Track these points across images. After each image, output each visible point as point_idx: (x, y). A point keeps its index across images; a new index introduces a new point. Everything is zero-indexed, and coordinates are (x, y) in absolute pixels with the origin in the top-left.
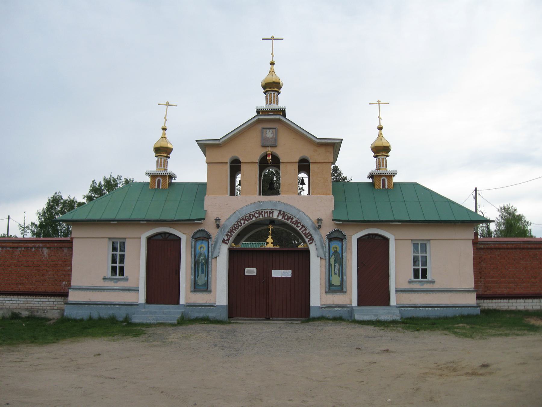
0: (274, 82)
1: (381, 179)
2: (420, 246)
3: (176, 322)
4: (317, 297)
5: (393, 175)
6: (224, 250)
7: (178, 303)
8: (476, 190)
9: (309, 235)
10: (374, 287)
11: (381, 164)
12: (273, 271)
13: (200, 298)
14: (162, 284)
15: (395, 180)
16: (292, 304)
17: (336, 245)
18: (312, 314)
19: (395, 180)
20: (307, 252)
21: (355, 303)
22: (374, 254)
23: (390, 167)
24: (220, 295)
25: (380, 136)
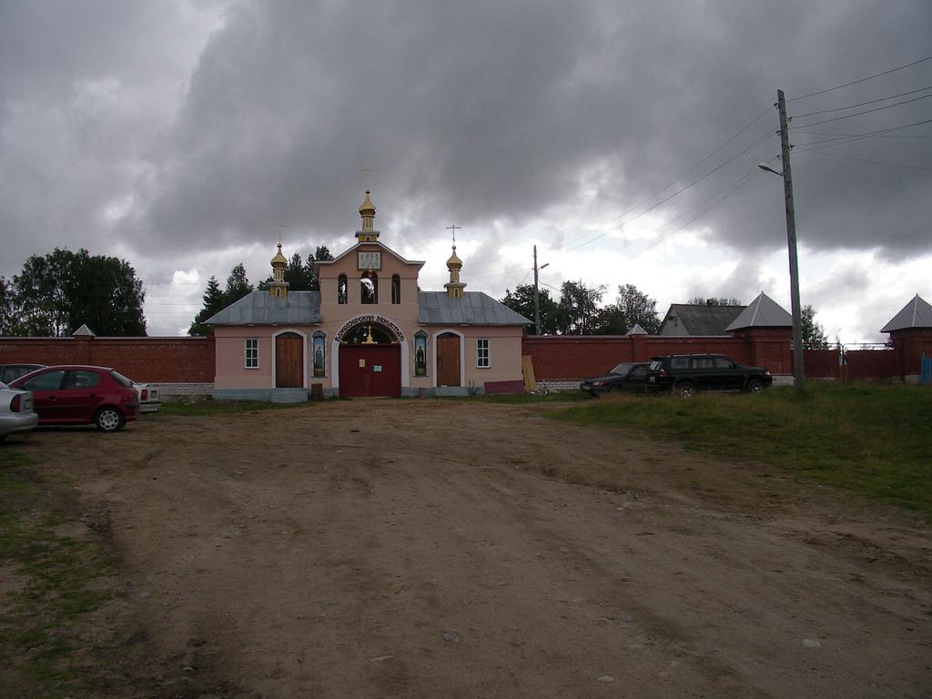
0: (370, 210)
1: (454, 288)
2: (483, 343)
3: (306, 399)
4: (407, 379)
5: (465, 285)
6: (335, 346)
7: (460, 385)
8: (535, 247)
9: (399, 334)
10: (449, 373)
11: (454, 276)
12: (184, 332)
13: (422, 383)
14: (288, 375)
15: (465, 290)
16: (389, 386)
17: (420, 343)
18: (403, 394)
19: (465, 290)
20: (398, 347)
21: (435, 385)
22: (449, 344)
23: (461, 281)
24: (333, 381)
25: (454, 254)
